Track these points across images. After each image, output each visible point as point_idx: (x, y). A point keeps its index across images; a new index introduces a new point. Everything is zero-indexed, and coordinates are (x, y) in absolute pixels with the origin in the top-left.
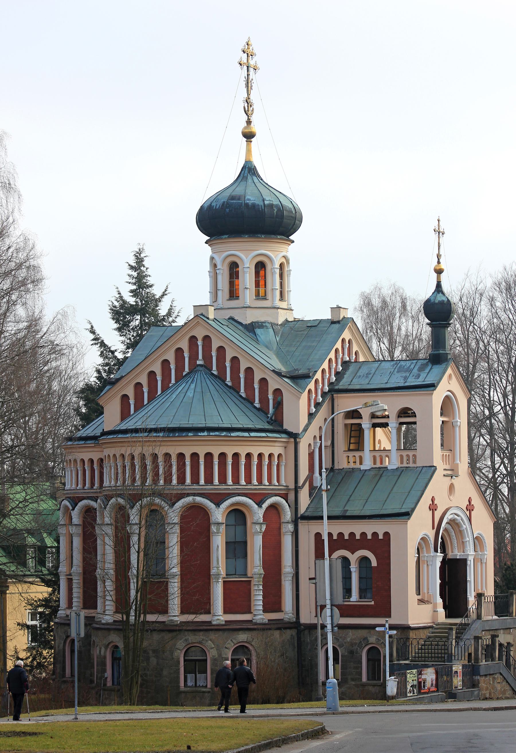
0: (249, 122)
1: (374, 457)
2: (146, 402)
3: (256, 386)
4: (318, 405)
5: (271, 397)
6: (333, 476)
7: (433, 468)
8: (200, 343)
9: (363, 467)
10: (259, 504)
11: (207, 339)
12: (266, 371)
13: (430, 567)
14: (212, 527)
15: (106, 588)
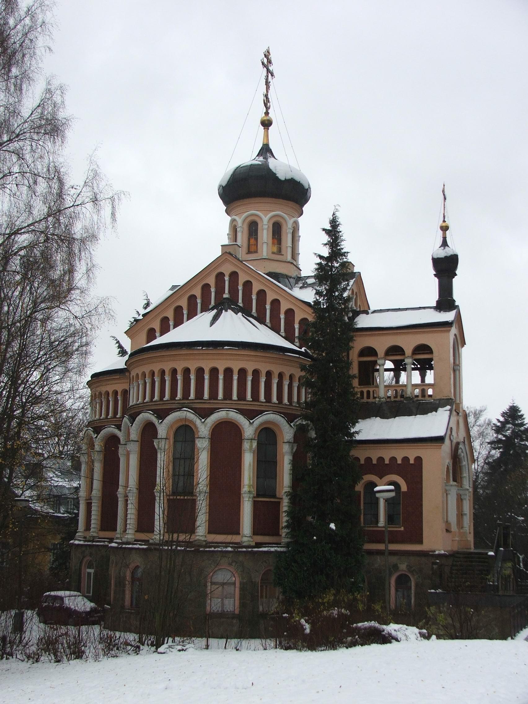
0: (267, 113)
8: (227, 278)
11: (234, 275)
13: (449, 496)
14: (245, 443)
15: (128, 512)
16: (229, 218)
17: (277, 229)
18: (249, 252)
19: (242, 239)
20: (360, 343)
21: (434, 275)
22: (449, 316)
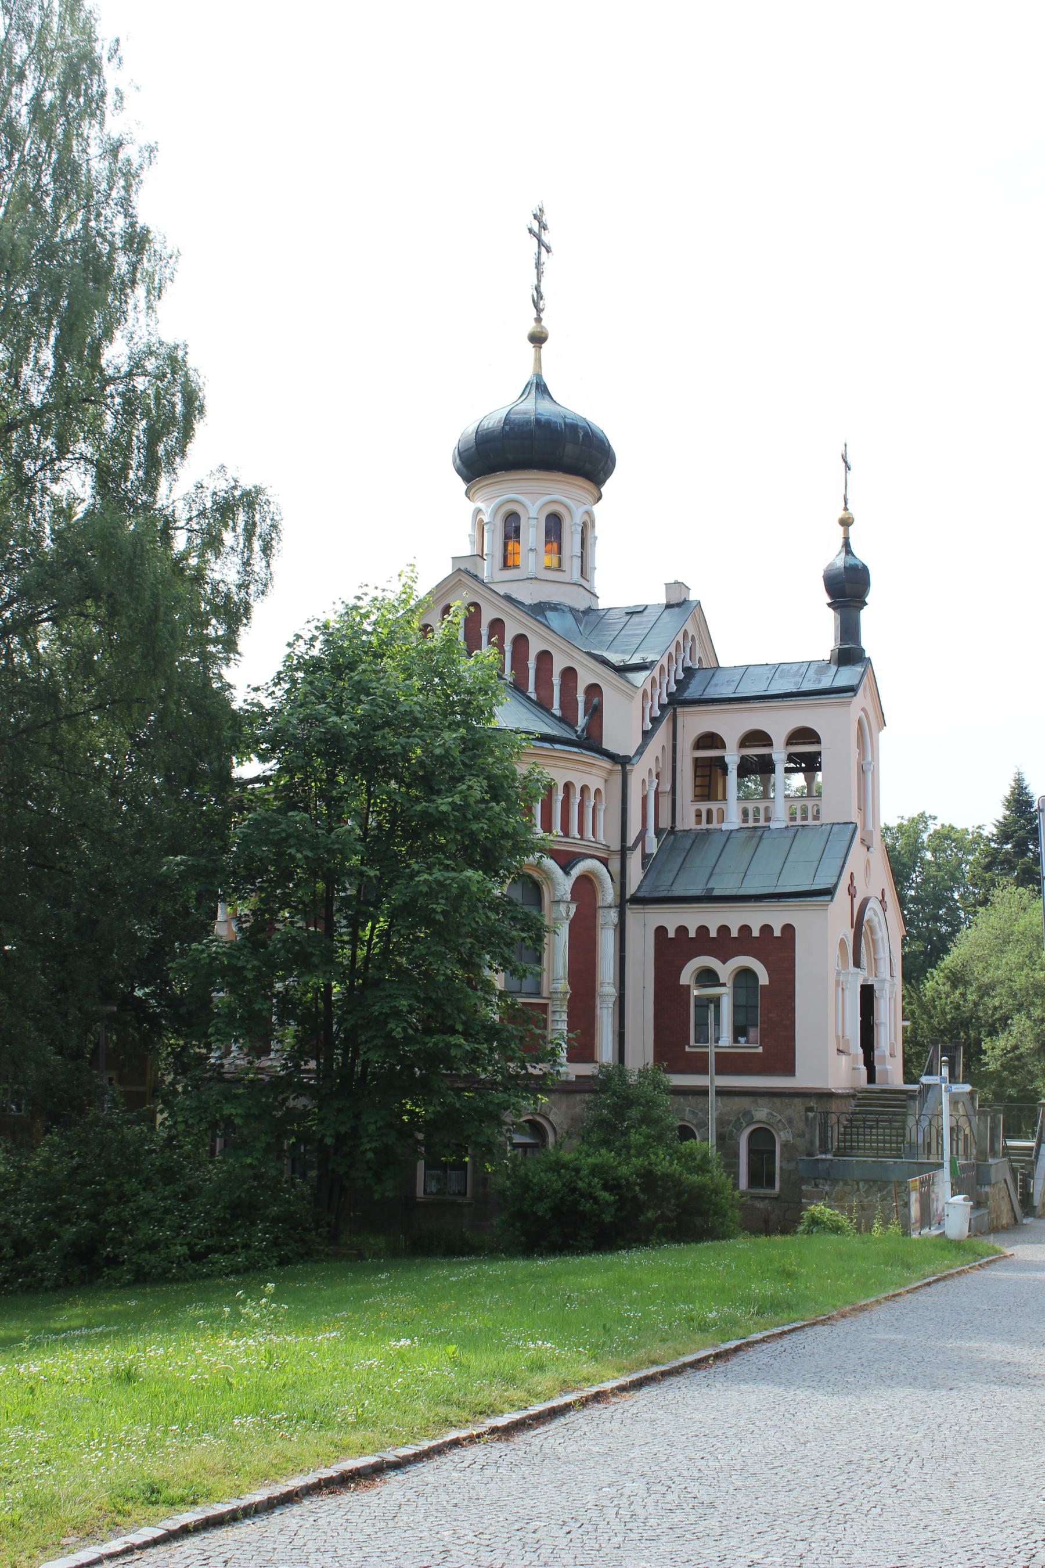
0: (538, 320)
1: (745, 812)
3: (556, 680)
4: (654, 721)
5: (581, 697)
6: (675, 840)
7: (851, 826)
9: (725, 827)
10: (566, 869)
12: (576, 654)
17: (554, 525)
18: (506, 565)
19: (493, 543)
21: (829, 605)
22: (846, 676)
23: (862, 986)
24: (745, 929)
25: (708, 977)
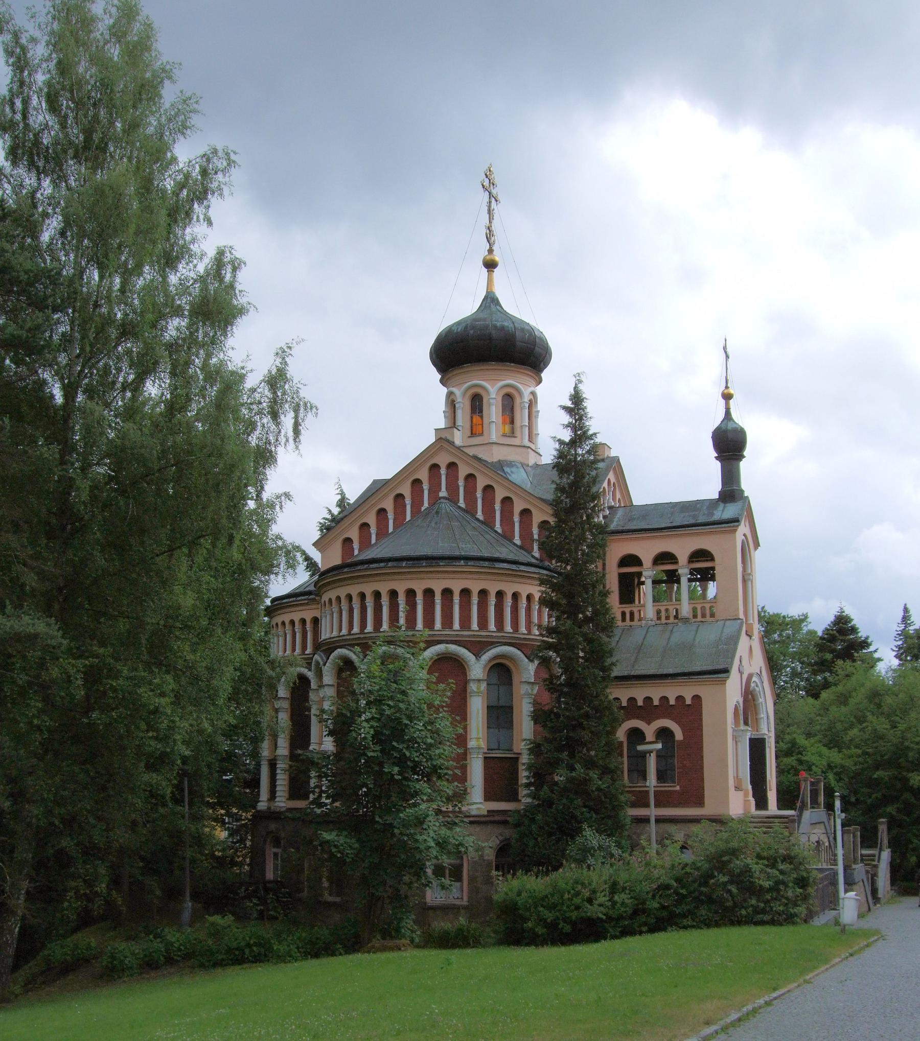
0: (491, 251)
2: (373, 541)
8: (443, 471)
13: (739, 744)
16: (444, 390)
18: (473, 434)
19: (463, 416)
20: (617, 550)
23: (750, 739)
24: (664, 699)
25: (636, 736)
